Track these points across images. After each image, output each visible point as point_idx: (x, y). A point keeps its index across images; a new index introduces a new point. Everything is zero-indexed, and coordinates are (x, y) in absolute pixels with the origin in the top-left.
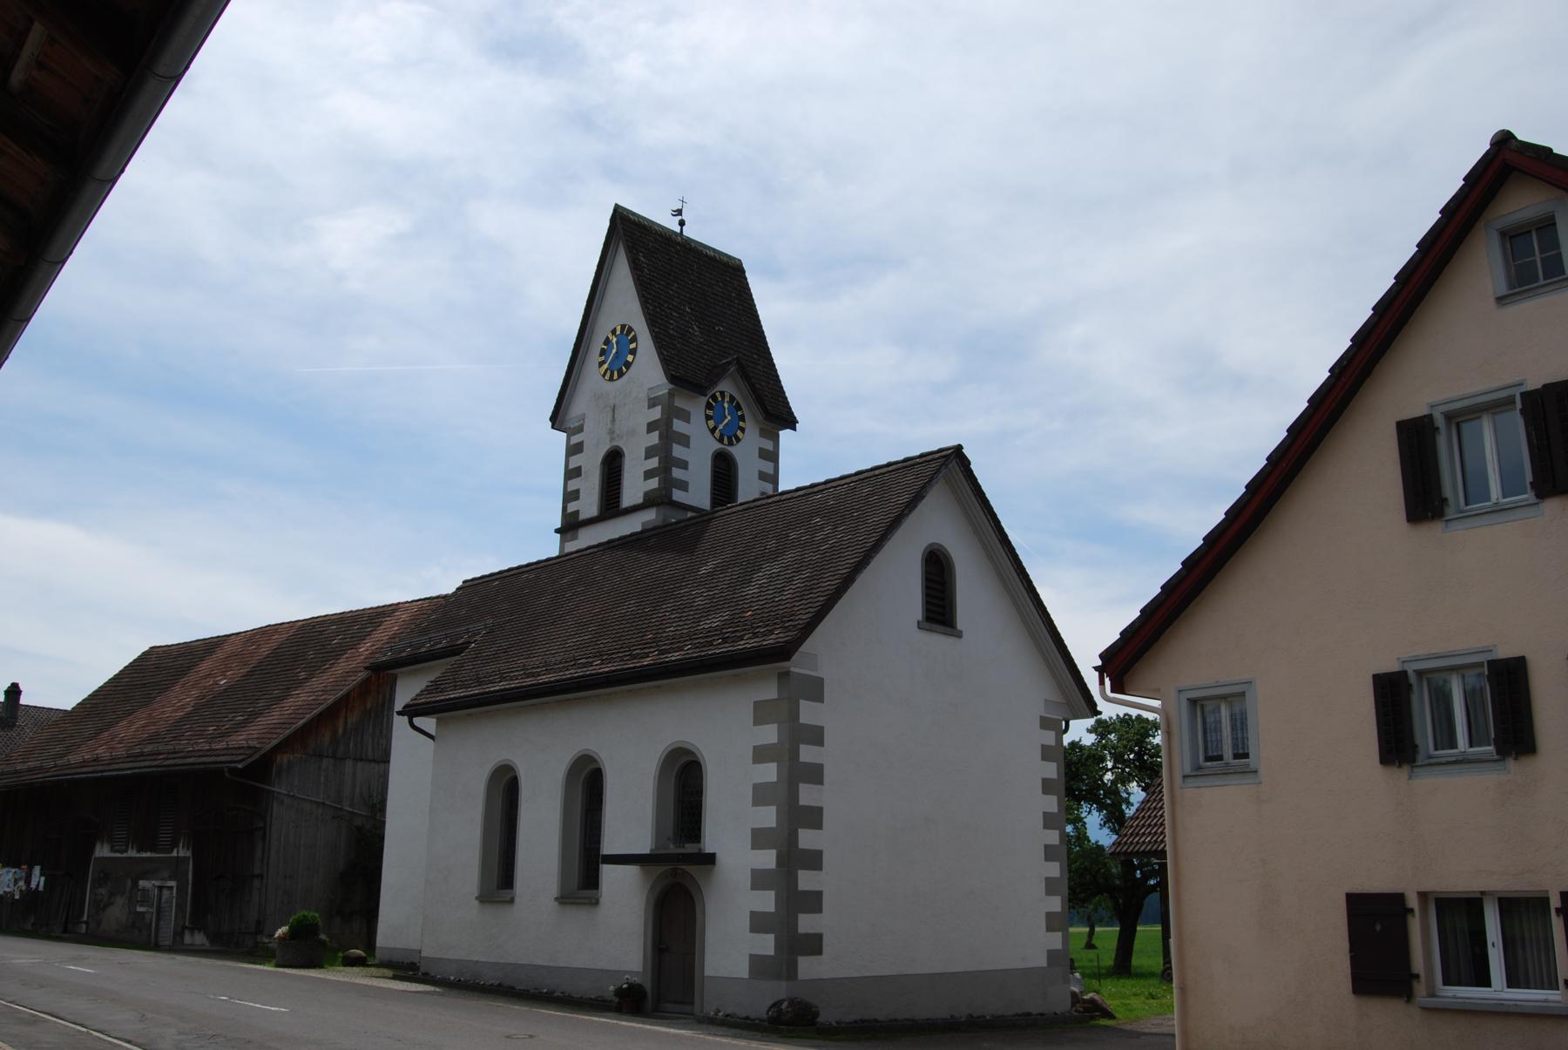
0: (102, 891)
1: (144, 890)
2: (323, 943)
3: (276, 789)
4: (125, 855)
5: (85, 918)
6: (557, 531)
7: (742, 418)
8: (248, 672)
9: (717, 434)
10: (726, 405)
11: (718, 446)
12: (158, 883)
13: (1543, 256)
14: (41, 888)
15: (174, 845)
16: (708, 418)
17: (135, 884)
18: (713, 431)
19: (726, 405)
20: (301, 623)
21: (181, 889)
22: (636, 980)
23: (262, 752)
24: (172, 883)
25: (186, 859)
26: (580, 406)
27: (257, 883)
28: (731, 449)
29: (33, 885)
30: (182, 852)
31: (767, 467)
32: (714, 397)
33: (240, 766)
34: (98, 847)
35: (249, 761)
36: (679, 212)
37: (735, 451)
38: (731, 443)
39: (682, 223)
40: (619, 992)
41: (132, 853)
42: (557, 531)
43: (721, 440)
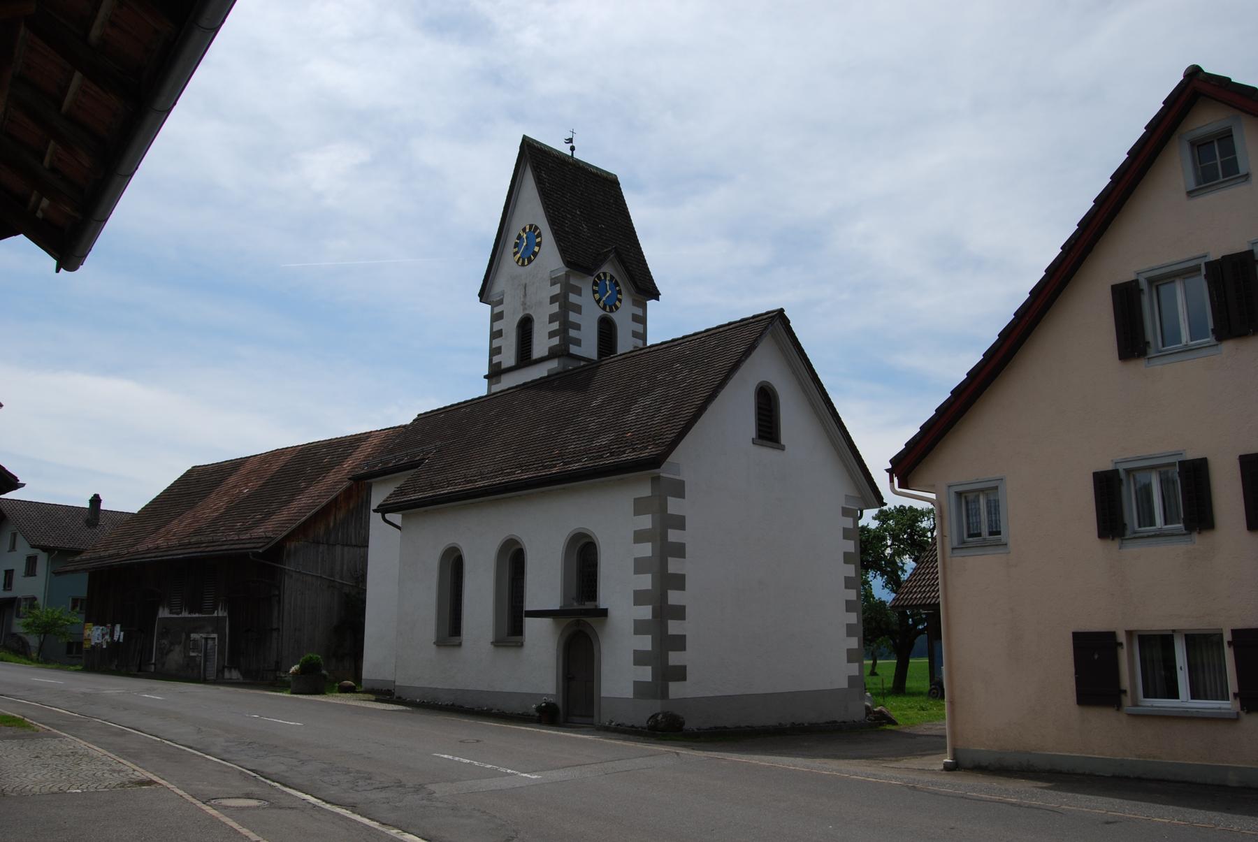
2: (325, 676)
3: (286, 567)
4: (180, 616)
5: (153, 661)
6: (485, 377)
10: (608, 283)
11: (602, 313)
12: (204, 636)
14: (121, 640)
15: (215, 608)
16: (595, 292)
17: (188, 637)
18: (598, 302)
19: (608, 283)
21: (221, 639)
22: (552, 700)
24: (215, 636)
27: (275, 634)
29: (116, 638)
30: (221, 613)
32: (599, 277)
36: (570, 140)
38: (611, 311)
39: (573, 149)
40: (539, 709)
41: (185, 614)
43: (604, 309)
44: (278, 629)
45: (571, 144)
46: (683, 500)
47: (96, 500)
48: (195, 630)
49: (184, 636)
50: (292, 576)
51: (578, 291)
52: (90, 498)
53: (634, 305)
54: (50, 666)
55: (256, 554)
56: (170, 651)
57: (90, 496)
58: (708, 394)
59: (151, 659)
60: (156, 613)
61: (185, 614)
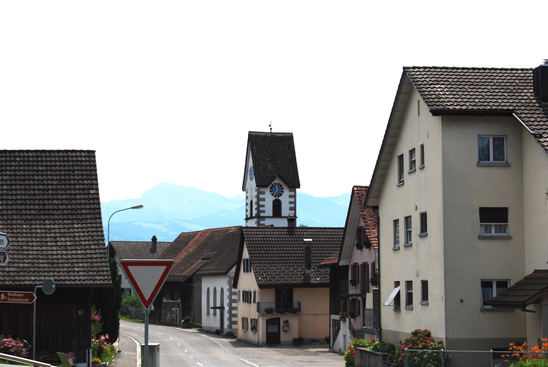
0: (165, 311)
1: (173, 311)
2: (191, 324)
3: (194, 285)
4: (169, 301)
5: (163, 318)
6: (245, 219)
7: (283, 188)
8: (197, 247)
9: (274, 195)
10: (276, 187)
11: (274, 198)
12: (175, 309)
13: (34, 357)
14: (153, 310)
15: (177, 299)
16: (271, 191)
17: (171, 309)
18: (273, 195)
19: (276, 187)
20: (213, 230)
21: (180, 311)
22: (218, 329)
23: (188, 277)
24: (178, 309)
25: (180, 302)
26: (247, 187)
27: (192, 309)
28: (280, 198)
29: (152, 309)
30: (179, 301)
31: (292, 200)
32: (273, 186)
33: (183, 281)
34: (164, 299)
35: (185, 279)
36: (270, 126)
37: (280, 198)
38: (279, 196)
39: (271, 129)
40: (216, 331)
41: (170, 301)
42: (245, 219)
43: (275, 196)
44: (193, 307)
45: (270, 127)
46: (509, 208)
47: (154, 239)
48: (173, 307)
49: (170, 309)
50: (196, 288)
51: (263, 193)
52: (152, 238)
53: (289, 191)
54: (132, 320)
55: (182, 282)
56: (167, 315)
57: (151, 237)
58: (208, 268)
59: (162, 318)
60: (162, 300)
61: (170, 301)
